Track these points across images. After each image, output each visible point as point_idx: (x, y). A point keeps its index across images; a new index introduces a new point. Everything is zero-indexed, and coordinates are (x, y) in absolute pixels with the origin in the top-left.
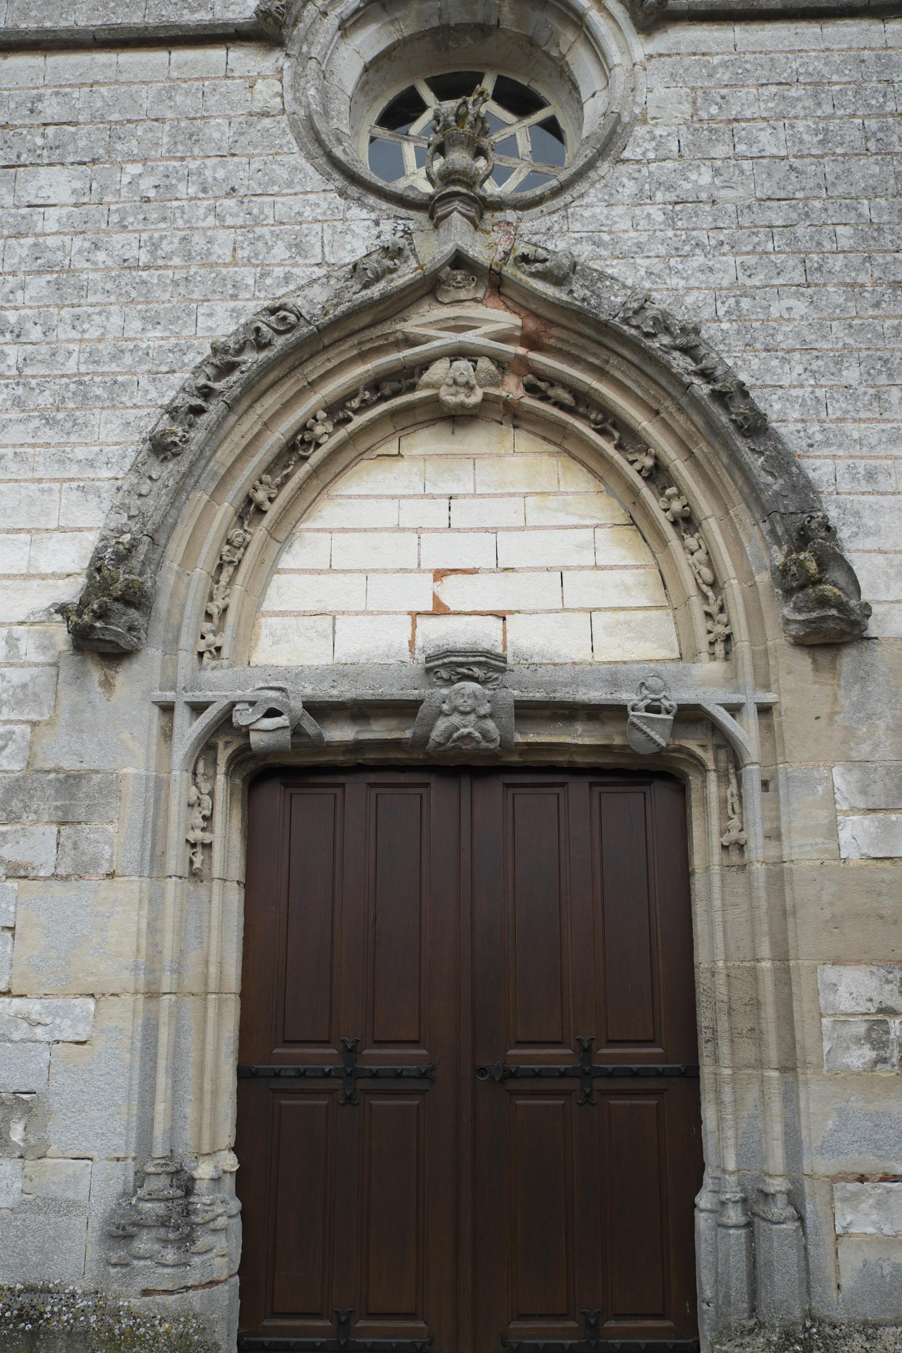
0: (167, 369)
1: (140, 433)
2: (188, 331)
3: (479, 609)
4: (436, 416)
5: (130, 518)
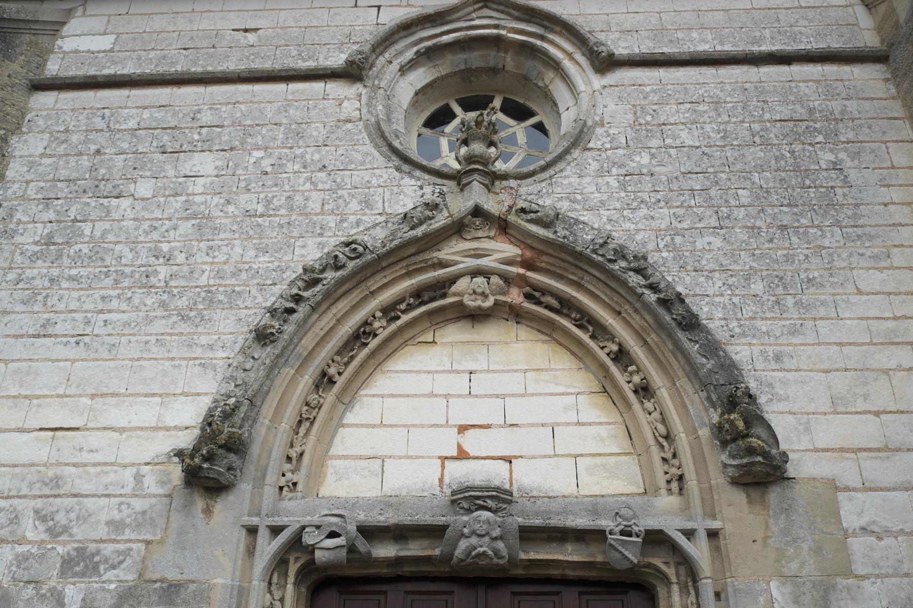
3: (492, 454)
4: (461, 315)
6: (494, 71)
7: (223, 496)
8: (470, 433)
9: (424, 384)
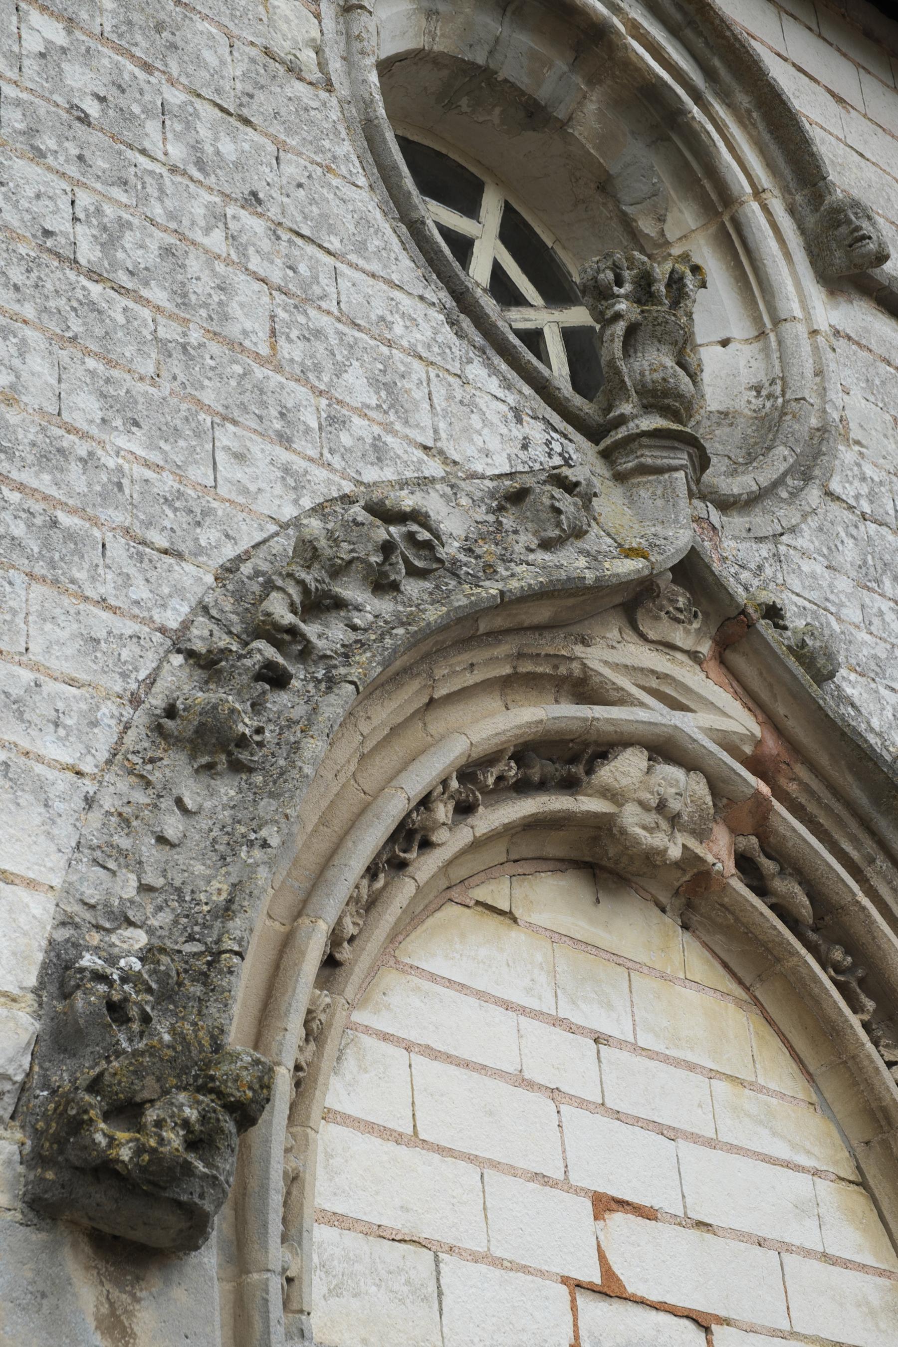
0: (165, 544)
1: (124, 675)
2: (200, 473)
3: (671, 1300)
4: (574, 855)
5: (145, 889)
6: (533, 114)
7: (155, 1282)
8: (618, 1218)
9: (491, 1037)
